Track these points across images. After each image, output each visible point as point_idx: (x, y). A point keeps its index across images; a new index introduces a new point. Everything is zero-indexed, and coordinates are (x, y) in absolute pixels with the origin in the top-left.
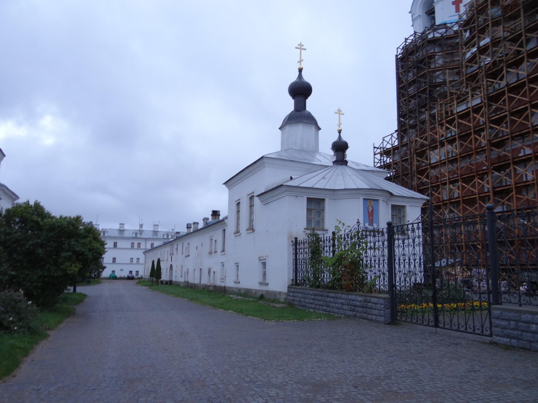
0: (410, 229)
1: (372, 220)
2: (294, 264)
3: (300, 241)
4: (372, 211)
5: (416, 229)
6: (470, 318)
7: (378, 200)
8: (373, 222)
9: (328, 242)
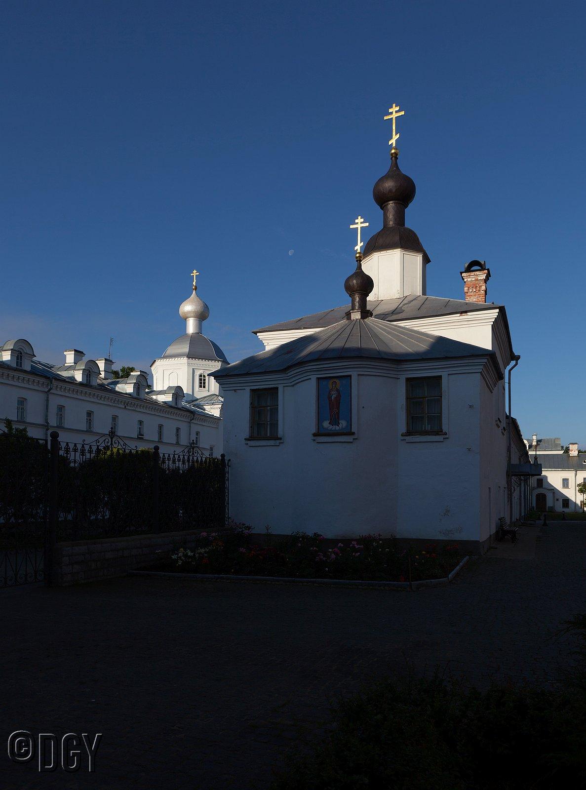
0: (63, 449)
1: (338, 413)
2: (227, 498)
3: (166, 456)
4: (339, 397)
5: (71, 450)
6: (407, 302)
7: (350, 376)
8: (338, 418)
9: (171, 462)
